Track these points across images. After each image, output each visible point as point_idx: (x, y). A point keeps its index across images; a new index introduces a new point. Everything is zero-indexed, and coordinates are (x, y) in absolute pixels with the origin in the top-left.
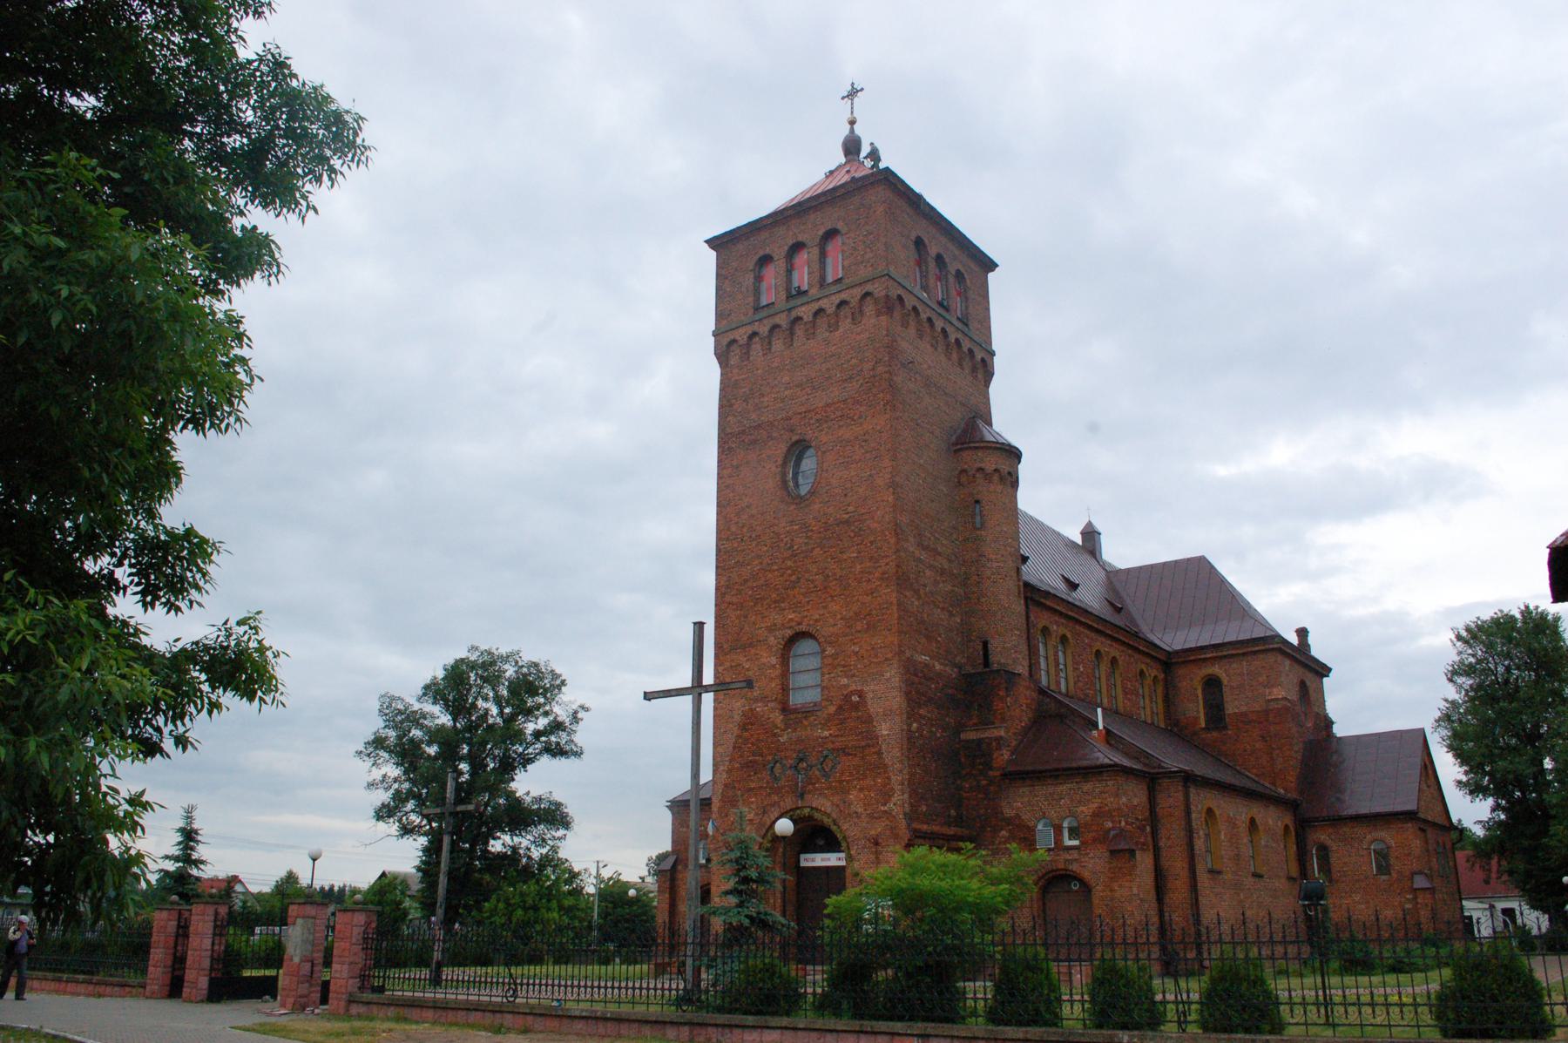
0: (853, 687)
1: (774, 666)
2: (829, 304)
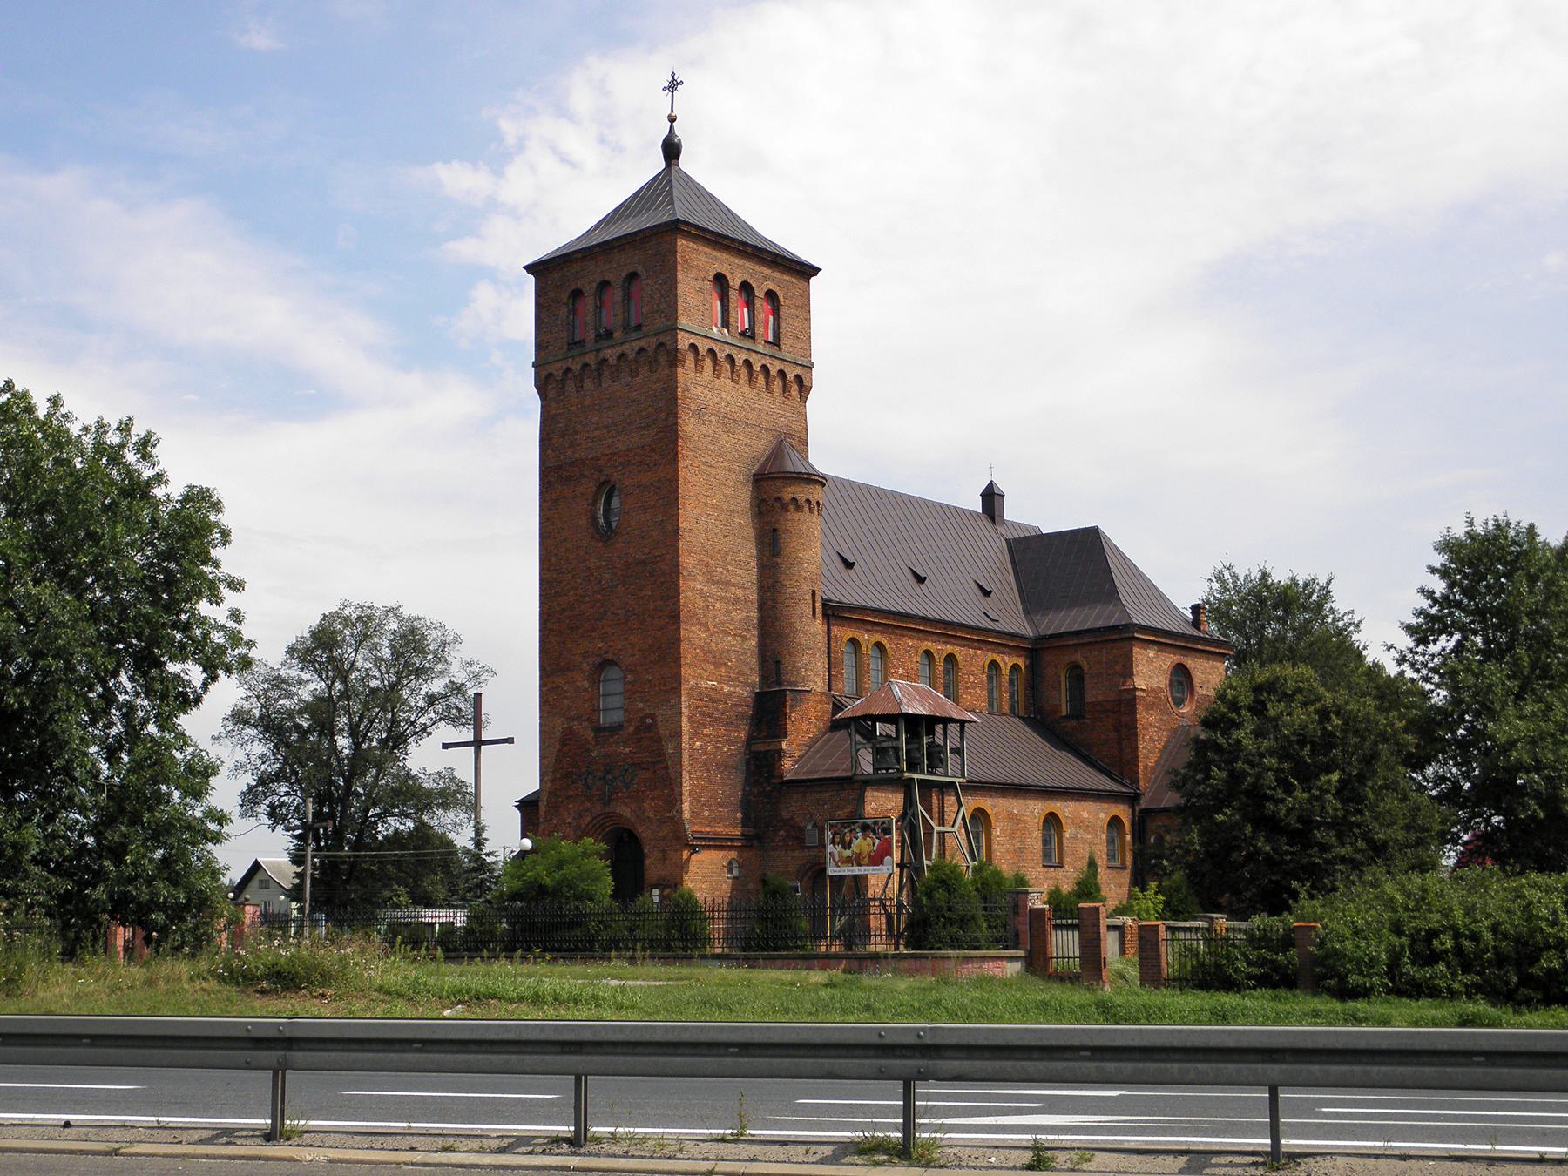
0: (647, 712)
2: (630, 349)
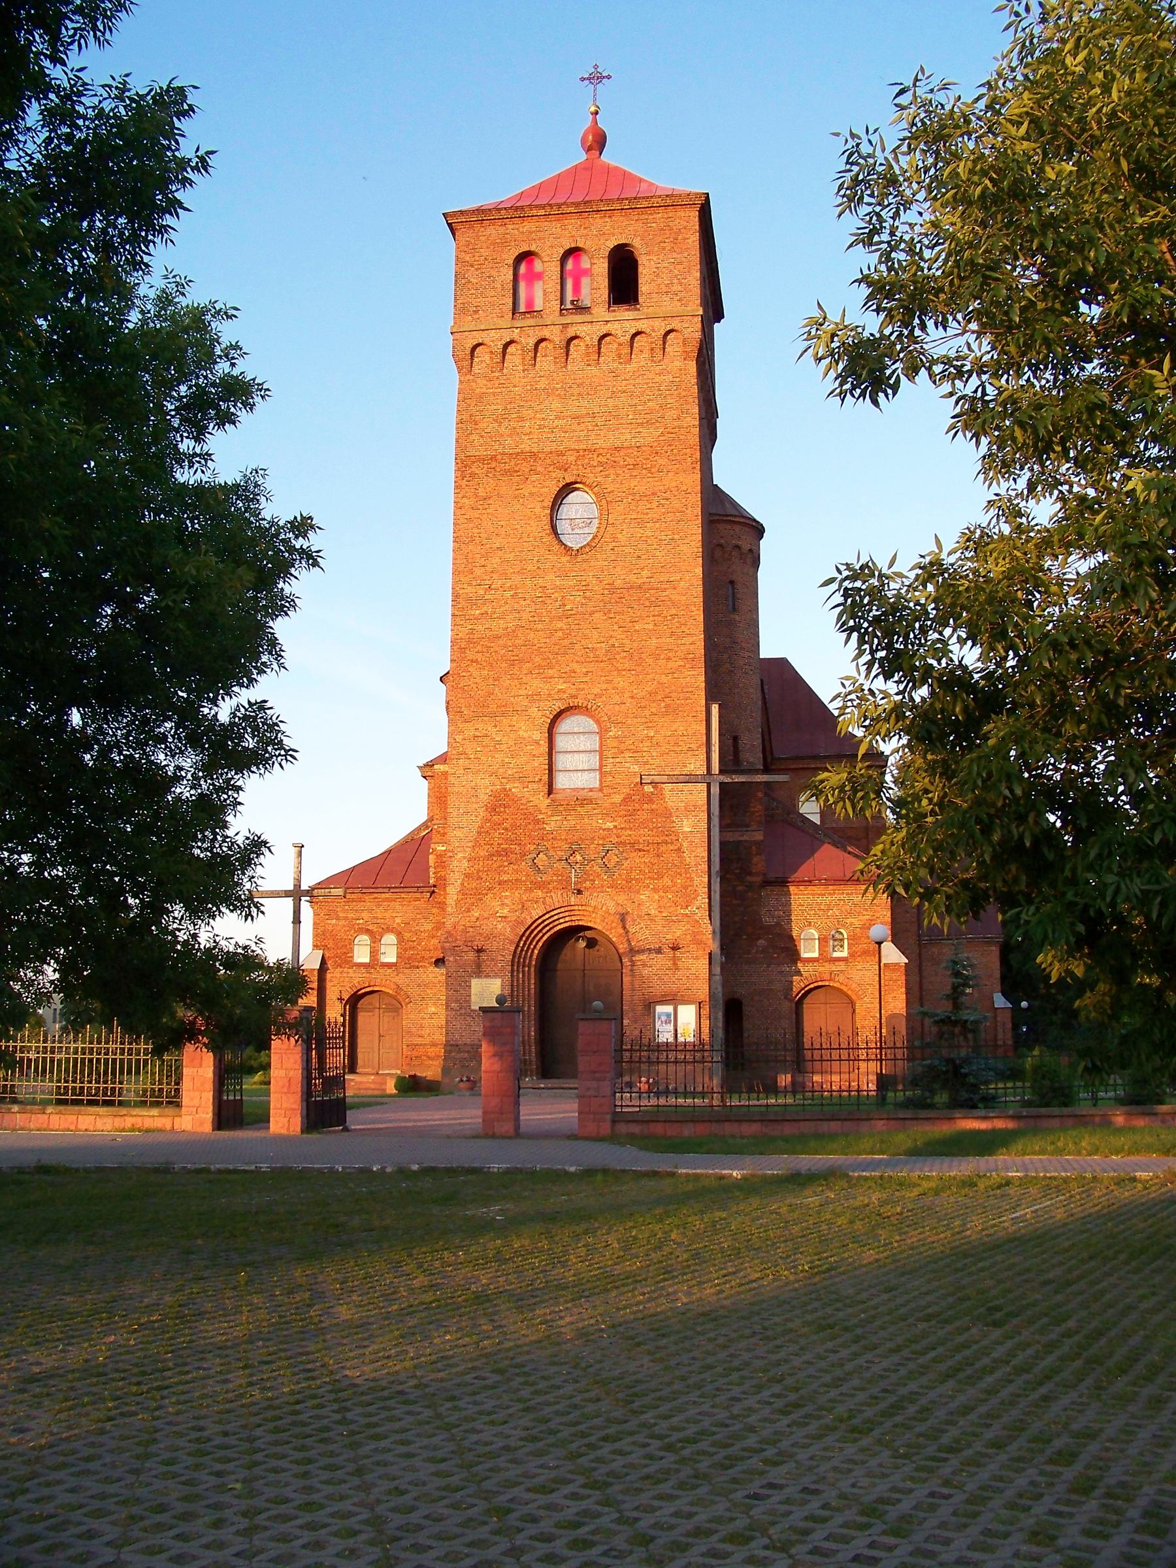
1: (537, 743)
